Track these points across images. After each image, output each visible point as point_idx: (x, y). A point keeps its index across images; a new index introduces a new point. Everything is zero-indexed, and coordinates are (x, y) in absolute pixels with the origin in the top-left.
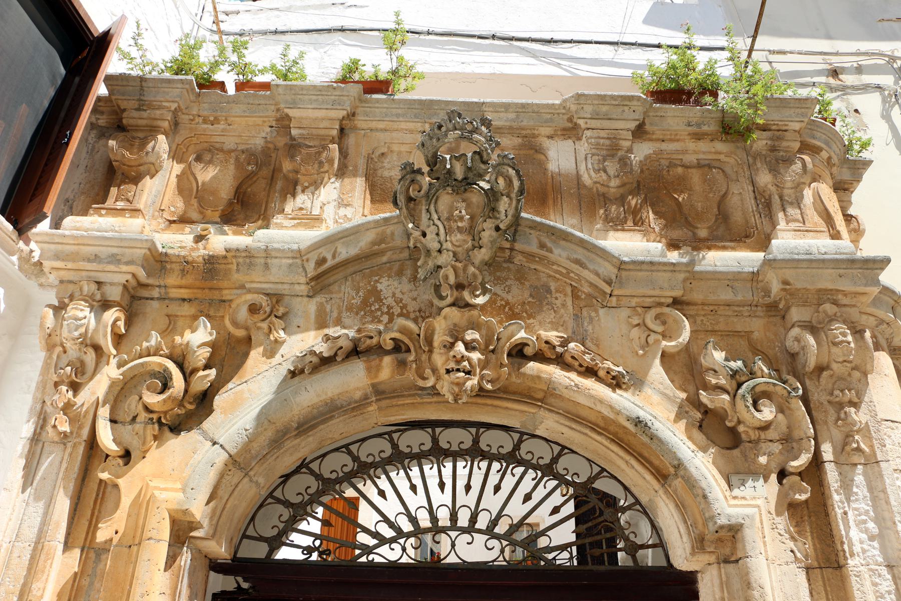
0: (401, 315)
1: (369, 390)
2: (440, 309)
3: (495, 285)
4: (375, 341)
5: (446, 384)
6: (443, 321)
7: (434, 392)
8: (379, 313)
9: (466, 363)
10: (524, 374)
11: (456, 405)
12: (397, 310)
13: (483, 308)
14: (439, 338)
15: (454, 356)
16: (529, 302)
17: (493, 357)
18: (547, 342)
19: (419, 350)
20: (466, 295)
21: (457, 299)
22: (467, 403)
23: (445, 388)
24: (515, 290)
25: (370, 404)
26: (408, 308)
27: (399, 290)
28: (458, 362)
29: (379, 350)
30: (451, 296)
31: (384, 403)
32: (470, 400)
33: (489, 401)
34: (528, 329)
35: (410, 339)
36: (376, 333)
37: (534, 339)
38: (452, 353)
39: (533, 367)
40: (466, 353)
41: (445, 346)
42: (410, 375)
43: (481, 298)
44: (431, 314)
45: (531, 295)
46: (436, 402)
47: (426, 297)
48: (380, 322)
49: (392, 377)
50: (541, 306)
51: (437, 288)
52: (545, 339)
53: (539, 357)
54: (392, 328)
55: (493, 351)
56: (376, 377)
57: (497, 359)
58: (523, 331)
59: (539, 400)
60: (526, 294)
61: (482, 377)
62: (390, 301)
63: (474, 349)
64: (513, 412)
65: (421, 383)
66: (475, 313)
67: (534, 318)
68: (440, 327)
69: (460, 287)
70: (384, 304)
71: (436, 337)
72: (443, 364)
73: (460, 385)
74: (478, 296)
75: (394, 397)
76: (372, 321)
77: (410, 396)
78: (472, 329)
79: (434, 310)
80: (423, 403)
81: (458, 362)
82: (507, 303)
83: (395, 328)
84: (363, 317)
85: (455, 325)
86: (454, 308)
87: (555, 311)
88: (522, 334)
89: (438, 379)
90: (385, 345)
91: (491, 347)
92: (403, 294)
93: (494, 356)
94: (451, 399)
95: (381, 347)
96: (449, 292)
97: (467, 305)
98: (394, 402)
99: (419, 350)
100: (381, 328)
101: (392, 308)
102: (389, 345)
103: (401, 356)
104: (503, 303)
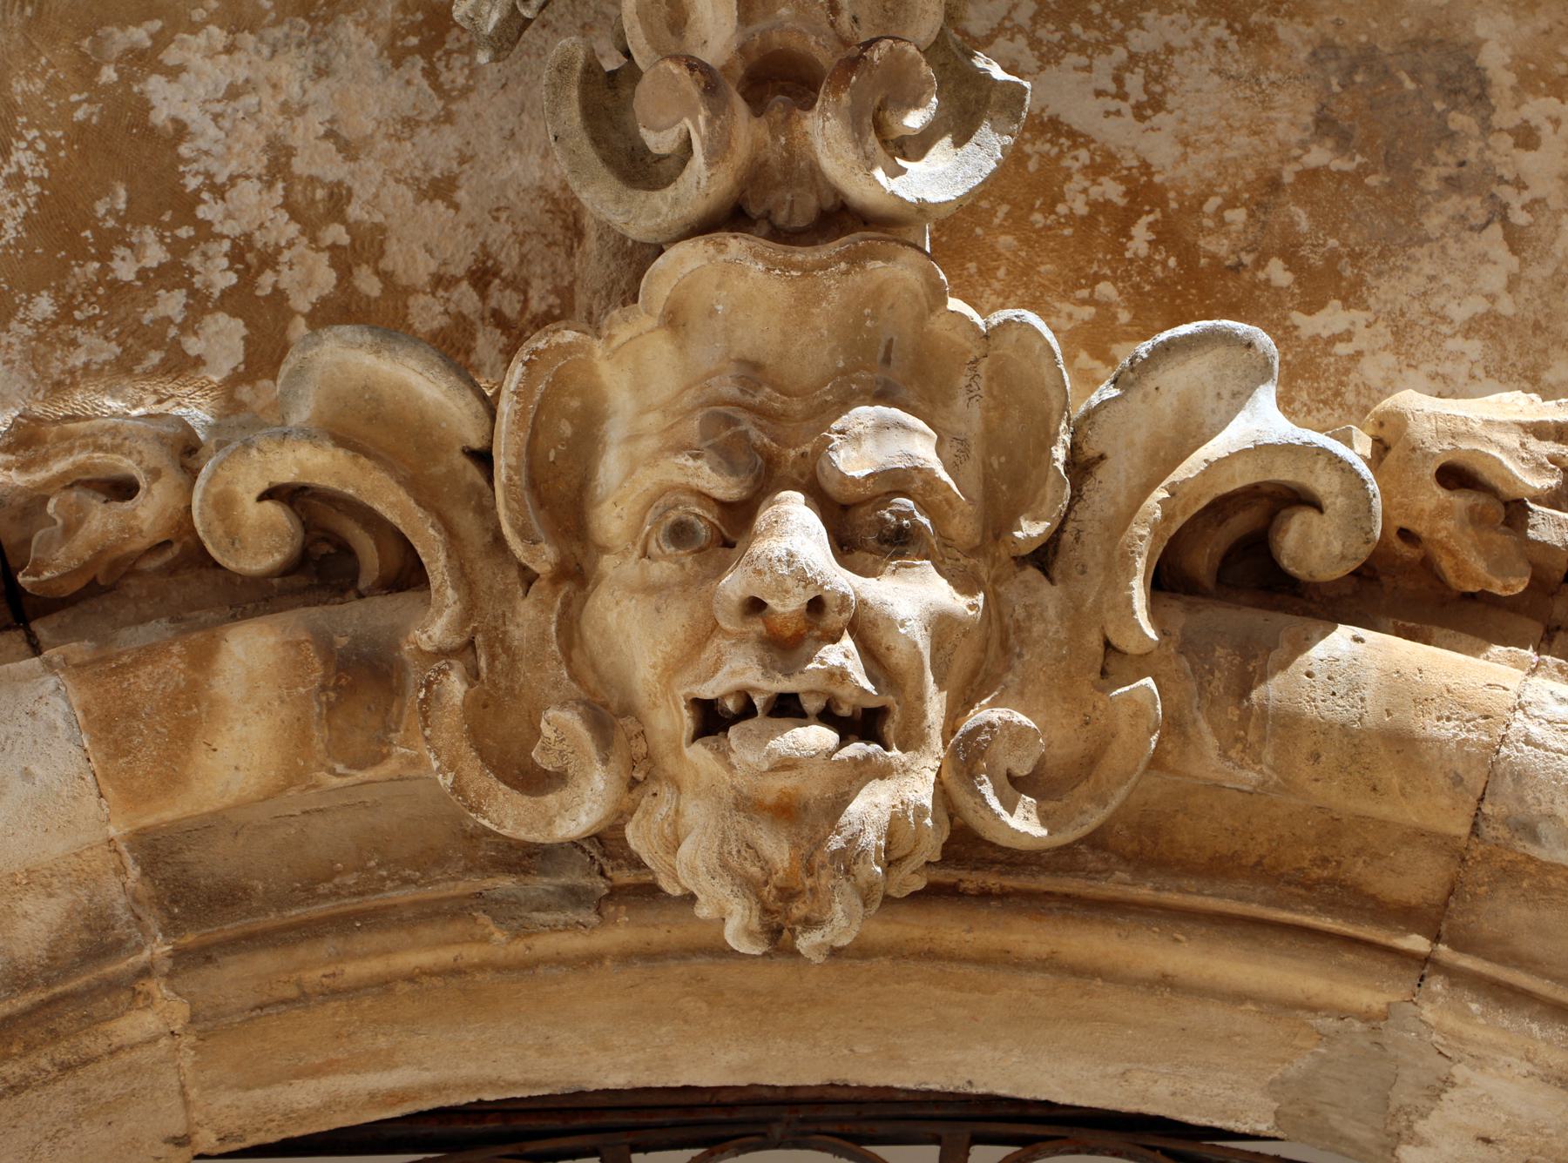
0: (340, 310)
1: (121, 886)
2: (638, 258)
3: (1048, 57)
4: (148, 512)
5: (696, 813)
6: (660, 352)
7: (610, 873)
8: (172, 304)
9: (841, 654)
10: (1288, 723)
11: (780, 970)
12: (307, 277)
13: (956, 232)
14: (631, 479)
15: (755, 606)
16: (1311, 176)
17: (1046, 599)
18: (1455, 476)
19: (485, 571)
20: (827, 140)
21: (756, 176)
22: (861, 951)
23: (692, 845)
24: (1201, 92)
25: (129, 989)
26: (395, 258)
27: (315, 123)
28: (785, 647)
29: (186, 581)
30: (715, 156)
31: (236, 979)
32: (885, 931)
33: (1028, 936)
34: (1309, 379)
35: (422, 490)
36: (155, 456)
37: (1358, 452)
38: (734, 584)
39: (1352, 660)
40: (842, 580)
41: (680, 533)
42: (430, 760)
43: (941, 156)
44: (566, 295)
45: (1325, 124)
46: (627, 957)
47: (525, 169)
48: (180, 366)
49: (293, 776)
50: (1403, 202)
51: (606, 96)
52: (1440, 449)
53: (1402, 588)
54: (280, 407)
55: (1044, 557)
56: (172, 779)
57: (1075, 615)
58: (1266, 397)
59: (1408, 916)
60: (1291, 114)
61: (968, 755)
62: (253, 209)
63: (898, 544)
64: (1216, 1013)
65: (510, 815)
66: (900, 272)
67: (1352, 296)
68: (641, 389)
69: (775, 79)
70: (206, 232)
71: (611, 468)
72: (673, 668)
73: (806, 813)
74: (917, 146)
75: (311, 931)
76: (124, 367)
77: (432, 913)
78: (883, 396)
79: (592, 265)
80: (527, 966)
81: (785, 647)
82: (1144, 191)
83: (302, 413)
84: (52, 335)
85: (752, 371)
86: (736, 245)
87: (1515, 240)
88: (1262, 421)
89: (641, 776)
90: (233, 537)
91: (1031, 530)
92: (348, 149)
93: (1049, 596)
94: (737, 924)
95: (197, 558)
96: (697, 126)
97: (839, 218)
98: (315, 964)
99: (485, 571)
100: (198, 412)
101: (269, 260)
102: (260, 542)
103: (353, 619)
104: (1112, 190)
